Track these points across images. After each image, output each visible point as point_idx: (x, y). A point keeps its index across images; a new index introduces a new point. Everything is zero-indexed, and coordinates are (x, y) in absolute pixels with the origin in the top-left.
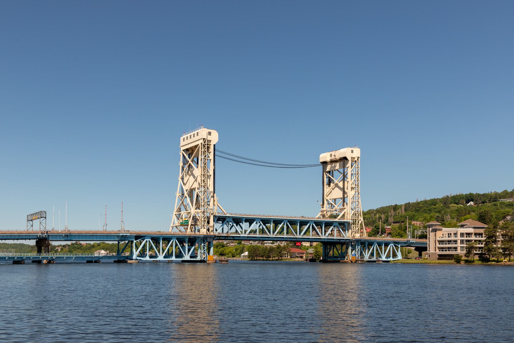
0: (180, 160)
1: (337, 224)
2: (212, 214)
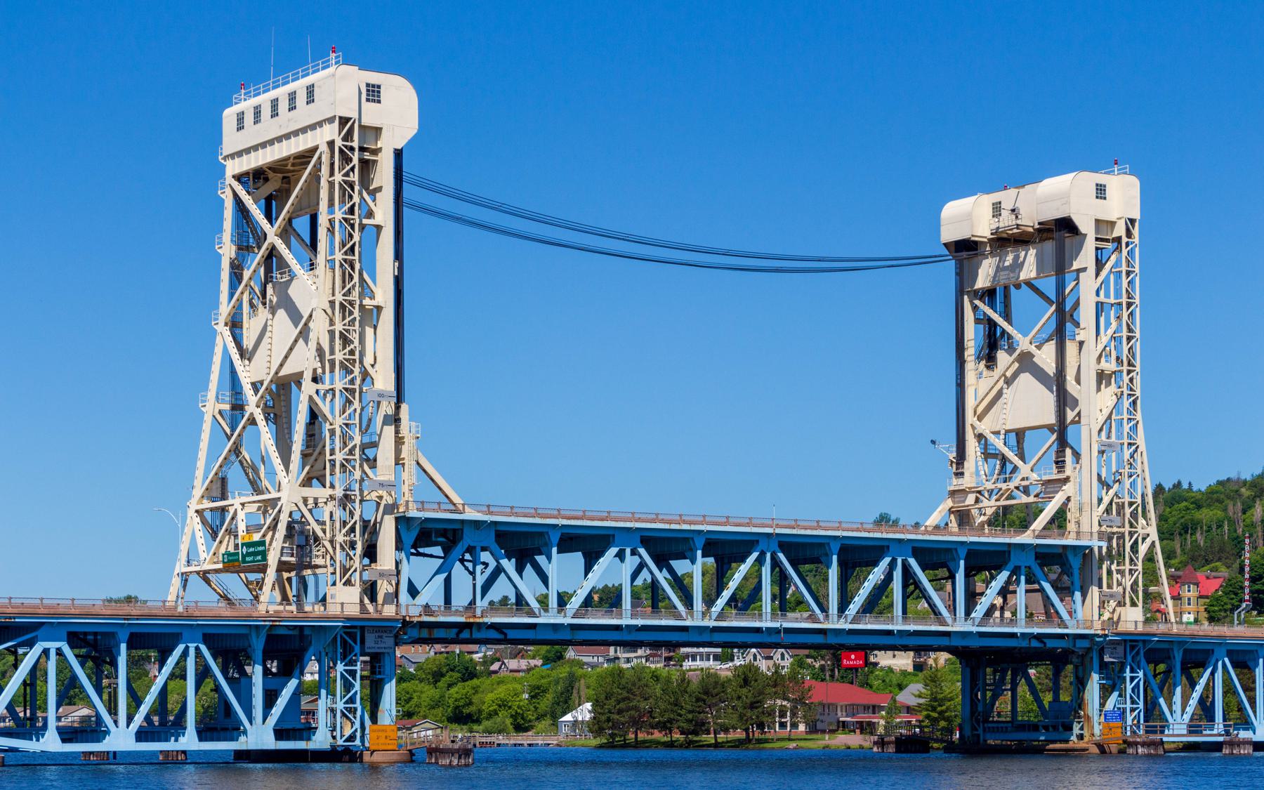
0: (221, 230)
1: (1029, 560)
2: (390, 509)
